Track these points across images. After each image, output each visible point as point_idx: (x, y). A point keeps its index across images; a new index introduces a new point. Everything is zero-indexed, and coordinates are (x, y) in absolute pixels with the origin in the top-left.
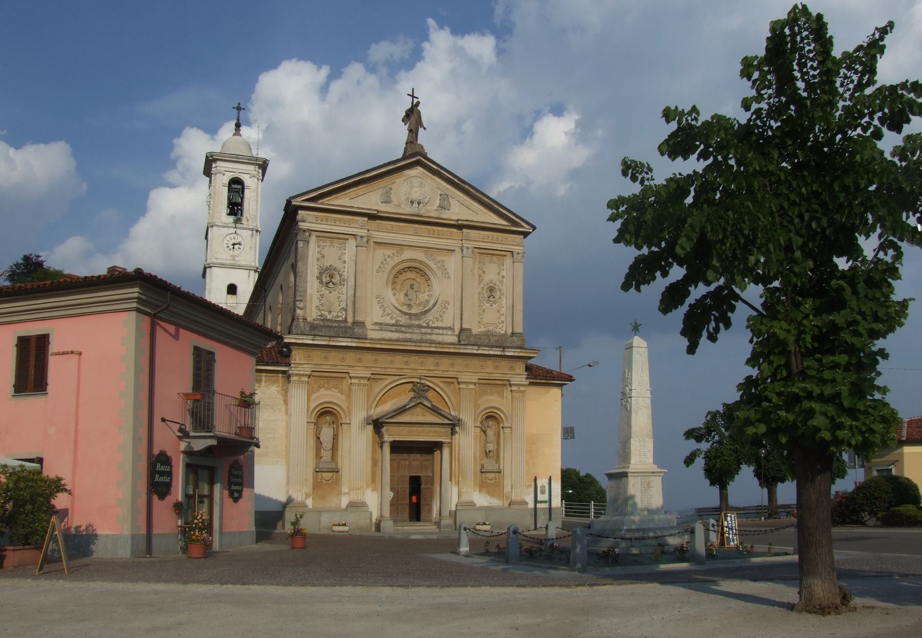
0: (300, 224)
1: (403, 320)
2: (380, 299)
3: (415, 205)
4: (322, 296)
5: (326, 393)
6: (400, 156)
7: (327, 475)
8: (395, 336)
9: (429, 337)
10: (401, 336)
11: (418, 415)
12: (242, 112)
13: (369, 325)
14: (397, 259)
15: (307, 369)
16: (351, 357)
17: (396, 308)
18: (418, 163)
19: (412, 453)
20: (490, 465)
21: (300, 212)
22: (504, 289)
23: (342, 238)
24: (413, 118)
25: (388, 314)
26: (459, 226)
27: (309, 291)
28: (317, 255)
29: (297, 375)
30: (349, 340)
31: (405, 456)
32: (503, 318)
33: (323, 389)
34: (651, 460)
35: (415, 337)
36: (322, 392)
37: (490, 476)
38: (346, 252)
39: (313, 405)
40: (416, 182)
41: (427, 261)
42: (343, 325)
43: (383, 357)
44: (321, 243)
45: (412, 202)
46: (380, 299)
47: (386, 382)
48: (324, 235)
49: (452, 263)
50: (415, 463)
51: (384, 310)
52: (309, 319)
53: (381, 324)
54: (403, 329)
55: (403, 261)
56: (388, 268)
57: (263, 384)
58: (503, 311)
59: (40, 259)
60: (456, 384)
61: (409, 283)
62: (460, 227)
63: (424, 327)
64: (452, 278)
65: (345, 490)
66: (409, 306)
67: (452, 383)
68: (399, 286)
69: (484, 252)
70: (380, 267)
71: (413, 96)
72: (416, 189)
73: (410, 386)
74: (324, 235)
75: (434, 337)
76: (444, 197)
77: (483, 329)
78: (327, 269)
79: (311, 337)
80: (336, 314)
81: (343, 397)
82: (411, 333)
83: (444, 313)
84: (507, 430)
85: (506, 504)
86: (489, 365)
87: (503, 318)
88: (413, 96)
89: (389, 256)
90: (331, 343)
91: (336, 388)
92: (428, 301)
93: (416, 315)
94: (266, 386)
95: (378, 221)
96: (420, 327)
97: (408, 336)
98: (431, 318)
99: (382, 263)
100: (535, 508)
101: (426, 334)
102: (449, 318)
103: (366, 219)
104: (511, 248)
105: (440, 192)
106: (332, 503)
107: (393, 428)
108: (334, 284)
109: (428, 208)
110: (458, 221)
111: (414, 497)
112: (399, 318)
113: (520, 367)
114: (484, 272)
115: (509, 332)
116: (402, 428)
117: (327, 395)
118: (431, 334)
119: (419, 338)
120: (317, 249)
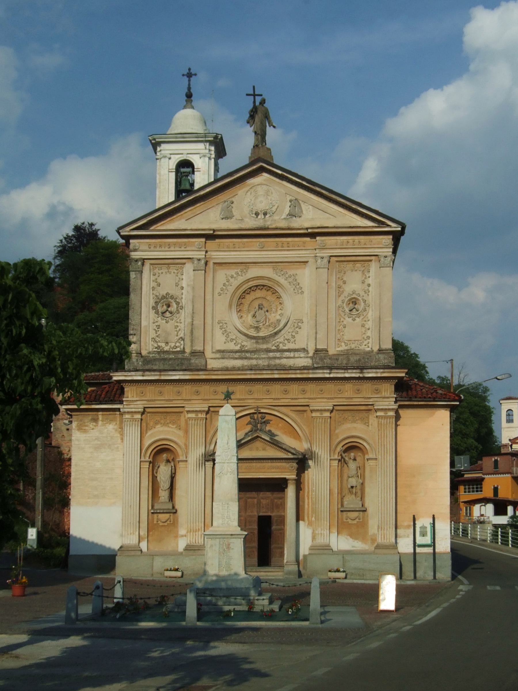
0: (132, 254)
1: (249, 345)
3: (261, 216)
4: (158, 327)
6: (247, 162)
7: (164, 517)
8: (238, 363)
10: (246, 363)
11: (257, 449)
12: (193, 79)
13: (209, 354)
14: (238, 279)
15: (139, 406)
16: (187, 390)
17: (240, 332)
18: (262, 170)
19: (261, 491)
20: (351, 502)
21: (131, 241)
23: (178, 263)
24: (258, 118)
25: (232, 340)
27: (144, 323)
28: (153, 284)
29: (128, 413)
30: (181, 373)
31: (254, 494)
32: (369, 333)
33: (159, 426)
34: (236, 523)
35: (262, 363)
36: (159, 428)
37: (350, 515)
38: (184, 277)
39: (147, 443)
40: (261, 190)
41: (277, 278)
42: (180, 356)
44: (156, 271)
45: (257, 214)
48: (159, 263)
49: (307, 276)
50: (264, 502)
51: (227, 336)
52: (144, 353)
53: (223, 351)
54: (248, 355)
55: (248, 280)
56: (231, 289)
57: (100, 423)
58: (369, 324)
59: (94, 228)
60: (309, 412)
61: (256, 304)
62: (313, 235)
63: (273, 351)
64: (306, 293)
65: (182, 531)
66: (257, 329)
67: (305, 411)
68: (246, 307)
69: (344, 259)
70: (222, 290)
71: (254, 95)
72: (261, 199)
73: (248, 419)
74: (159, 263)
75: (284, 361)
76: (295, 203)
78: (164, 297)
79: (140, 373)
80: (173, 344)
81: (181, 433)
84: (371, 463)
86: (348, 389)
87: (369, 333)
88: (254, 95)
89: (232, 277)
90: (163, 378)
91: (174, 424)
92: (279, 321)
93: (263, 338)
94: (103, 425)
95: (217, 240)
96: (268, 351)
97: (254, 362)
98: (281, 340)
99: (224, 285)
100: (415, 553)
101: (275, 358)
102: (305, 339)
103: (203, 240)
105: (289, 198)
106: (168, 546)
108: (171, 313)
109: (276, 217)
111: (264, 539)
112: (244, 343)
114: (345, 283)
115: (376, 349)
117: (161, 432)
118: (280, 358)
119: (266, 363)
120: (153, 278)
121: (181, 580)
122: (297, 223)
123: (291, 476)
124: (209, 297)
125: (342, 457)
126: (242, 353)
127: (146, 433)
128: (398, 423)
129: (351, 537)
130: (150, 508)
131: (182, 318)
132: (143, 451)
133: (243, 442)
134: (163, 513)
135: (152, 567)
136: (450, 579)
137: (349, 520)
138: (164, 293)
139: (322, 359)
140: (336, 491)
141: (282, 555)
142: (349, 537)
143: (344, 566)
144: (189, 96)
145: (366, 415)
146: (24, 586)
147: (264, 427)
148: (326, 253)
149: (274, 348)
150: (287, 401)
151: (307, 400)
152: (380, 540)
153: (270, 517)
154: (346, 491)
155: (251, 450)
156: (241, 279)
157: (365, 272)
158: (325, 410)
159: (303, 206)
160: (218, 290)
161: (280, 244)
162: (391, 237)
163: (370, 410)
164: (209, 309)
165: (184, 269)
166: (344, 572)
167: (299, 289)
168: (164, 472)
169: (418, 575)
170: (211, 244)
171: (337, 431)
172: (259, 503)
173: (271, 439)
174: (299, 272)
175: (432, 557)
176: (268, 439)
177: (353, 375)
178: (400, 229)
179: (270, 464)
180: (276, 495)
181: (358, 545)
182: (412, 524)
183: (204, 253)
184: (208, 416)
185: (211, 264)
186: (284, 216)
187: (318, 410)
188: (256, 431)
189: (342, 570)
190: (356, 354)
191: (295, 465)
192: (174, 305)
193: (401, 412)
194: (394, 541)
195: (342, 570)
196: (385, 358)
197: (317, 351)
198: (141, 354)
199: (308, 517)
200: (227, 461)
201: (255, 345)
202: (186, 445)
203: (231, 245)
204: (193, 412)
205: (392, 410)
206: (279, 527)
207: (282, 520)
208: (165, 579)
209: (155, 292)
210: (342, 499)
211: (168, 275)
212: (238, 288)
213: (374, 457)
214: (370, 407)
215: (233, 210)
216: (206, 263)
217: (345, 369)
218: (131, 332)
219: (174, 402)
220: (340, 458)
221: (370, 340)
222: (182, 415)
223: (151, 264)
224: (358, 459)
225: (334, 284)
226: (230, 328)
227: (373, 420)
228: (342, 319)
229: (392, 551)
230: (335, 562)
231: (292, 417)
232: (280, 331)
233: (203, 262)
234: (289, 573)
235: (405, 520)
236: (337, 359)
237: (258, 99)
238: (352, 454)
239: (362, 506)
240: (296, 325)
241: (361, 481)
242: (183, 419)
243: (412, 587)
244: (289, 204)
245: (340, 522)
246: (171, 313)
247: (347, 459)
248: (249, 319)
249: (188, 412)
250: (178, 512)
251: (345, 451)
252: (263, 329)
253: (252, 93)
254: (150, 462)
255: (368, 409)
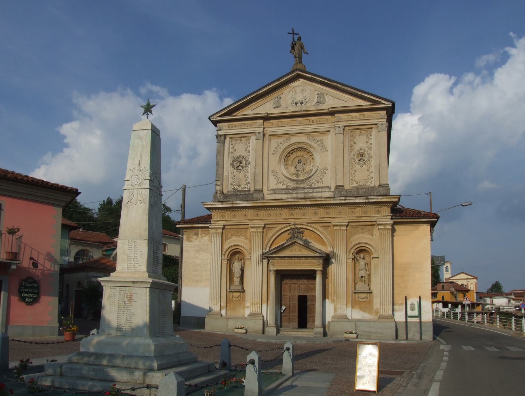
1: (292, 185)
2: (274, 173)
3: (299, 105)
5: (235, 239)
7: (236, 294)
8: (285, 196)
9: (310, 195)
10: (289, 196)
11: (295, 250)
13: (265, 191)
14: (284, 144)
15: (221, 224)
16: (250, 214)
18: (298, 77)
19: (300, 279)
20: (361, 286)
22: (372, 153)
23: (246, 136)
26: (332, 113)
27: (225, 173)
28: (231, 150)
29: (214, 228)
31: (295, 281)
32: (372, 175)
35: (300, 196)
36: (234, 238)
39: (226, 247)
40: (298, 90)
43: (273, 212)
44: (233, 142)
45: (296, 104)
46: (274, 173)
47: (277, 229)
49: (329, 140)
50: (302, 286)
51: (278, 180)
52: (225, 192)
54: (291, 191)
55: (291, 145)
56: (280, 151)
57: (200, 236)
60: (332, 226)
61: (297, 160)
63: (308, 188)
65: (248, 304)
66: (297, 175)
67: (329, 226)
68: (290, 162)
71: (293, 34)
72: (299, 94)
75: (315, 195)
76: (321, 96)
77: (355, 185)
78: (238, 158)
79: (220, 203)
81: (247, 241)
82: (296, 193)
83: (324, 176)
85: (376, 318)
86: (358, 211)
87: (372, 175)
88: (293, 34)
90: (234, 205)
91: (243, 235)
92: (311, 170)
93: (302, 181)
94: (202, 237)
95: (271, 121)
96: (304, 188)
98: (313, 181)
99: (276, 148)
101: (309, 193)
102: (330, 180)
103: (262, 121)
104: (375, 121)
105: (317, 92)
107: (276, 261)
108: (242, 167)
109: (308, 105)
110: (328, 108)
112: (289, 184)
113: (386, 211)
115: (377, 185)
116: (283, 261)
117: (235, 241)
119: (303, 196)
121: (244, 337)
122: (323, 107)
123: (318, 268)
124: (266, 156)
125: (355, 257)
126: (287, 190)
127: (226, 241)
128: (394, 234)
129: (361, 310)
130: (228, 288)
131: (249, 170)
132: (223, 253)
133: (285, 245)
134: (236, 292)
135: (228, 325)
136: (431, 340)
137: (360, 299)
138: (238, 155)
139: (340, 192)
140: (350, 279)
141: (314, 321)
142: (359, 310)
143: (356, 329)
145: (371, 228)
146: (74, 334)
147: (299, 236)
148: (341, 124)
149: (308, 186)
150: (316, 219)
151: (330, 219)
152: (381, 313)
153: (306, 296)
154: (358, 280)
155: (291, 251)
156: (286, 144)
157: (369, 135)
158: (342, 225)
159: (326, 97)
160: (271, 152)
161: (311, 121)
162: (385, 112)
163: (374, 225)
164: (265, 164)
165: (251, 140)
166: (355, 333)
167: (324, 149)
168: (237, 266)
169: (409, 336)
170: (267, 123)
171: (351, 240)
172: (299, 286)
173: (304, 243)
174: (324, 138)
175: (419, 324)
176: (302, 243)
177: (361, 201)
178: (391, 105)
179: (304, 260)
180: (310, 282)
181: (366, 316)
182: (404, 302)
183: (262, 129)
184: (265, 230)
185: (267, 136)
186: (314, 104)
187: (337, 225)
188: (294, 238)
189: (354, 332)
190: (363, 188)
191: (321, 261)
192: (244, 162)
193: (396, 227)
194: (391, 313)
195: (354, 332)
196: (383, 190)
197: (337, 187)
198: (223, 192)
199: (331, 297)
200: (137, 187)
201: (296, 185)
202: (250, 249)
203: (280, 123)
204: (254, 227)
205: (390, 224)
206: (312, 303)
207: (314, 298)
208: (235, 334)
209: (232, 155)
210: (355, 285)
211: (241, 144)
212: (284, 150)
213: (377, 256)
214: (374, 223)
215: (281, 102)
216: (264, 135)
217: (355, 197)
219: (242, 221)
220: (353, 257)
221: (373, 180)
222: (248, 230)
223: (230, 138)
224: (366, 258)
225: (348, 144)
226: (279, 175)
227: (376, 232)
228: (354, 167)
229: (390, 320)
230: (349, 327)
231: (319, 230)
232: (312, 175)
233: (262, 134)
234: (317, 333)
235: (400, 299)
236: (351, 192)
237: (296, 37)
238: (362, 255)
239: (369, 289)
240: (323, 172)
241: (368, 273)
242: (248, 232)
243: (404, 346)
244: (317, 96)
245: (353, 300)
246: (242, 167)
247: (358, 258)
248: (292, 170)
249: (252, 227)
250: (246, 292)
251: (357, 253)
252: (301, 175)
253: (292, 32)
254: (228, 260)
255: (372, 224)
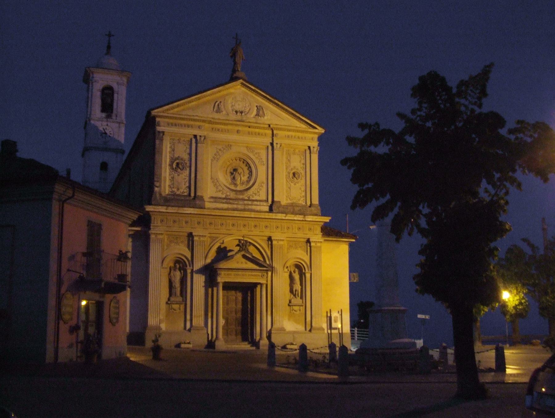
1: (232, 195)
8: (225, 206)
10: (230, 206)
12: (112, 38)
25: (220, 191)
51: (217, 188)
52: (163, 194)
53: (216, 198)
54: (231, 201)
76: (259, 109)
77: (289, 201)
82: (237, 204)
93: (240, 191)
97: (235, 206)
101: (248, 205)
112: (228, 194)
144: (109, 47)
149: (246, 198)
177: (299, 219)
186: (252, 116)
201: (235, 195)
218: (156, 179)
236: (287, 208)
